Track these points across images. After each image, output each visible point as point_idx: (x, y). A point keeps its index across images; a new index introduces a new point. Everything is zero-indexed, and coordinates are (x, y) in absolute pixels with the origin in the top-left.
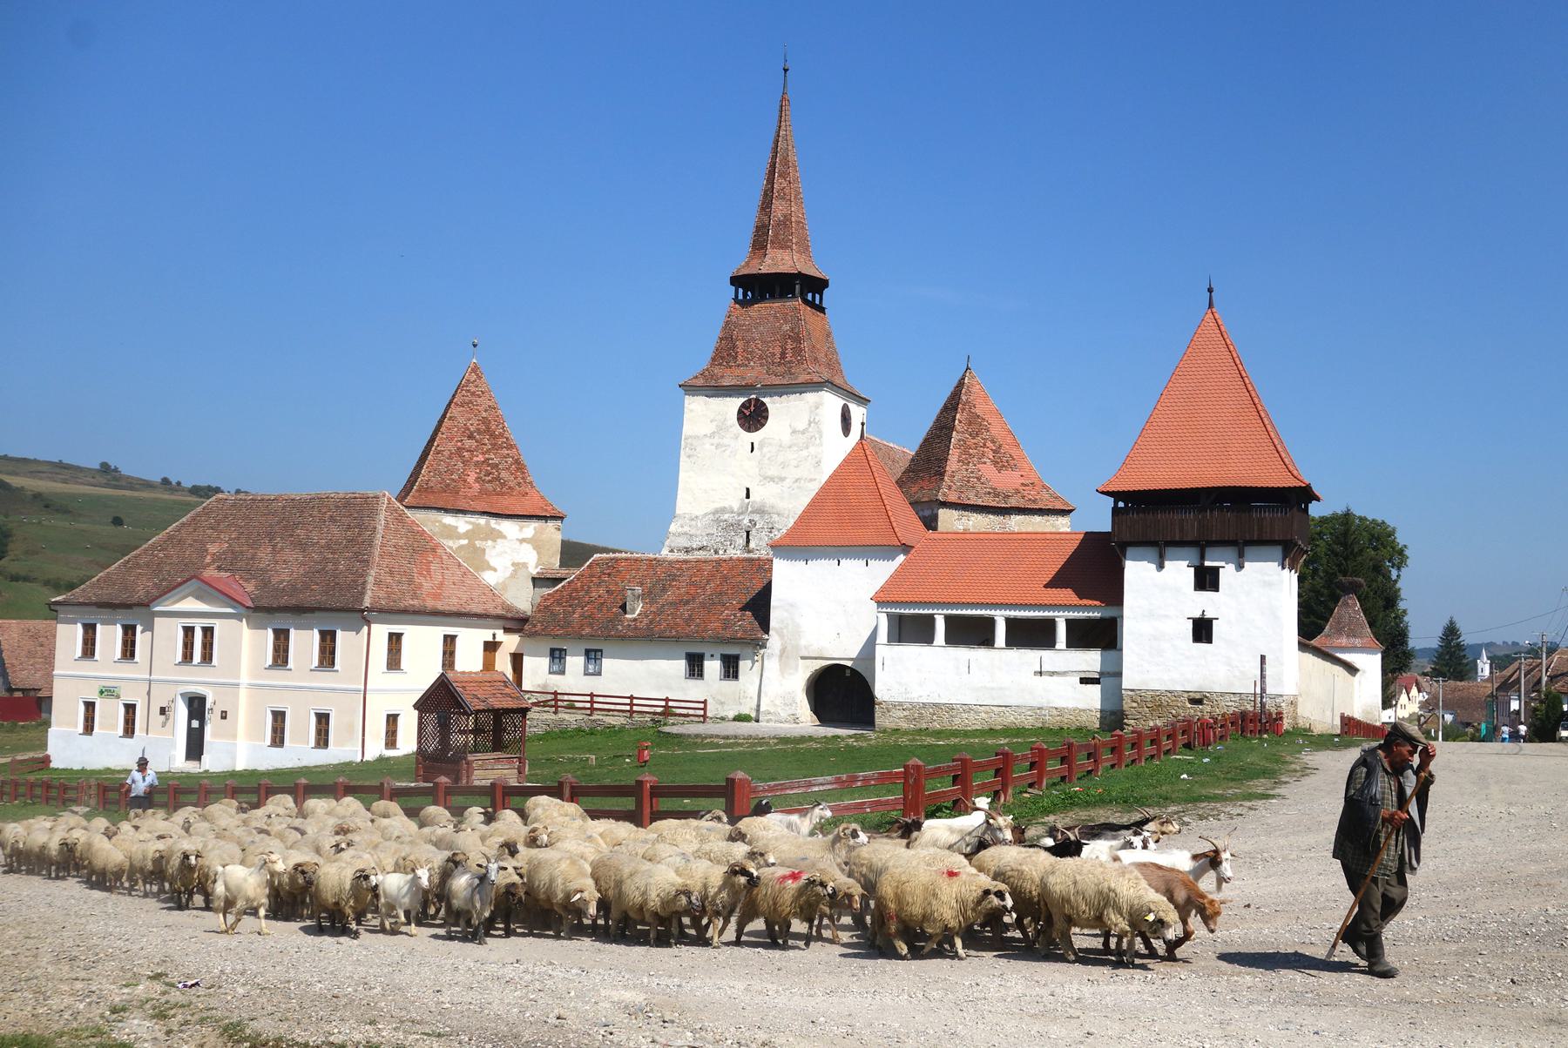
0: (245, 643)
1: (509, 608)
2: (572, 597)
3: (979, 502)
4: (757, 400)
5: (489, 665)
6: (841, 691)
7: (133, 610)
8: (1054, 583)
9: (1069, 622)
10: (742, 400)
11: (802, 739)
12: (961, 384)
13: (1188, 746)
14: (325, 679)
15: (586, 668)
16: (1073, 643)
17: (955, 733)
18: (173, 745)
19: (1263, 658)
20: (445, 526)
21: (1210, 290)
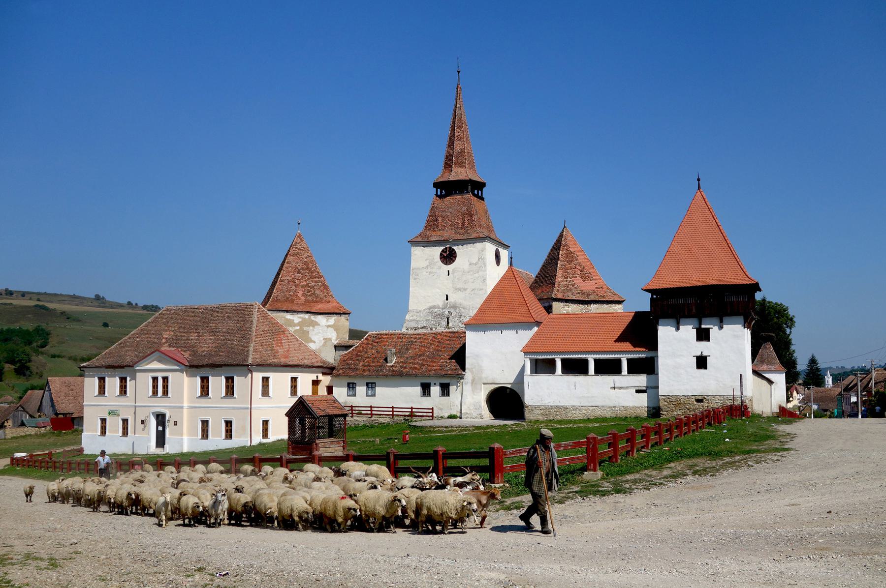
0: (185, 385)
1: (324, 362)
2: (358, 355)
3: (574, 298)
4: (450, 248)
5: (315, 392)
6: (506, 401)
7: (124, 369)
8: (620, 339)
9: (629, 360)
10: (442, 248)
11: (487, 427)
12: (561, 235)
13: (709, 424)
14: (229, 403)
15: (367, 393)
16: (631, 371)
17: (569, 422)
18: (149, 440)
19: (741, 375)
20: (287, 319)
21: (699, 180)
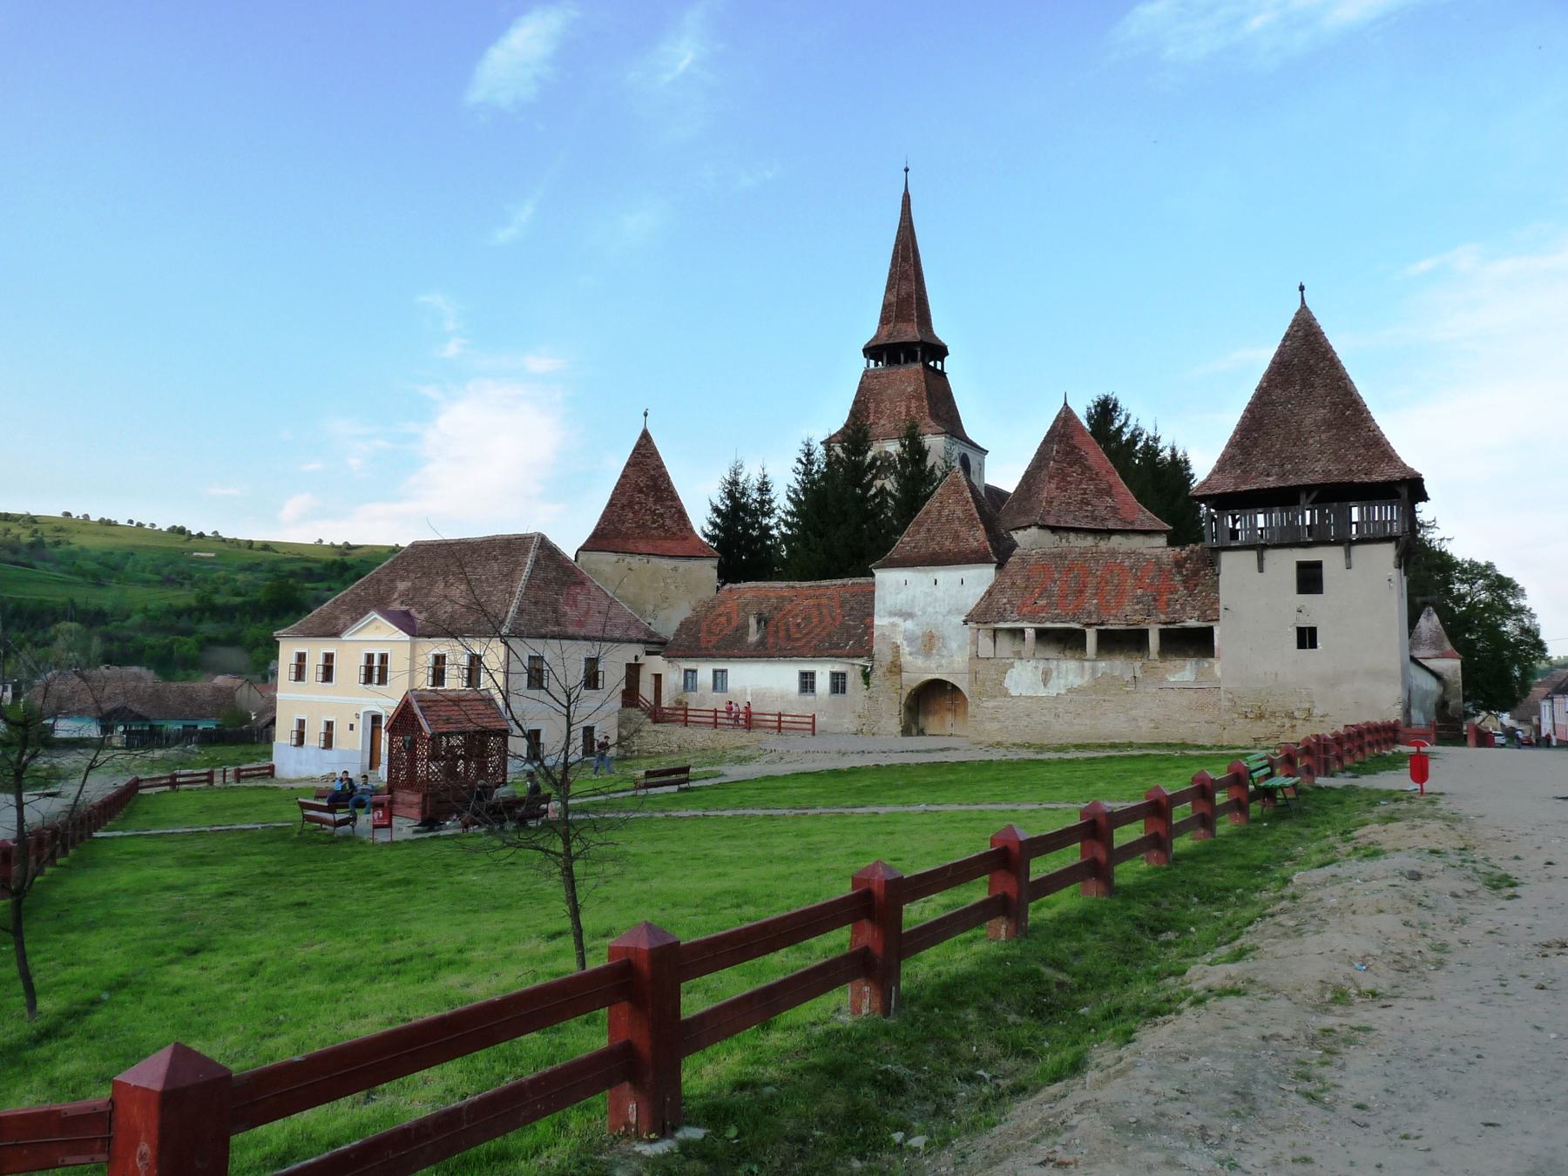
3: (1077, 525)
21: (1302, 288)
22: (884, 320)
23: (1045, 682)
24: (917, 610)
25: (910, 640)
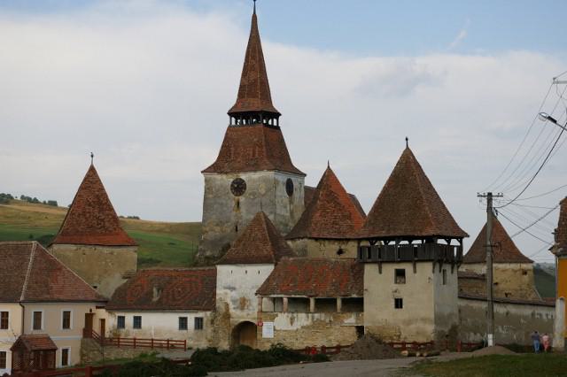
3: (329, 237)
21: (407, 139)
22: (241, 95)
23: (292, 323)
24: (237, 287)
25: (234, 301)
